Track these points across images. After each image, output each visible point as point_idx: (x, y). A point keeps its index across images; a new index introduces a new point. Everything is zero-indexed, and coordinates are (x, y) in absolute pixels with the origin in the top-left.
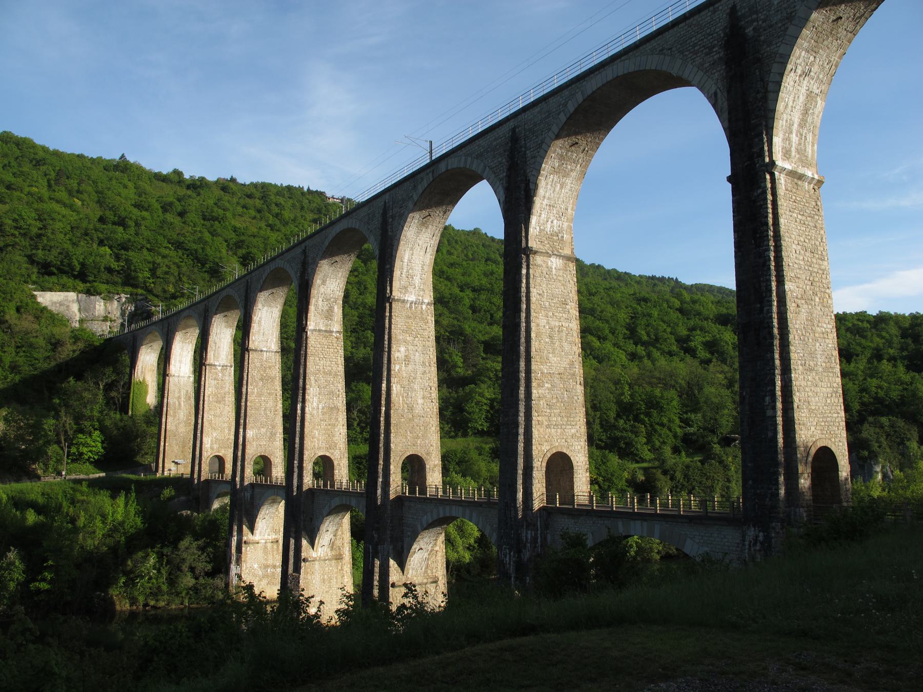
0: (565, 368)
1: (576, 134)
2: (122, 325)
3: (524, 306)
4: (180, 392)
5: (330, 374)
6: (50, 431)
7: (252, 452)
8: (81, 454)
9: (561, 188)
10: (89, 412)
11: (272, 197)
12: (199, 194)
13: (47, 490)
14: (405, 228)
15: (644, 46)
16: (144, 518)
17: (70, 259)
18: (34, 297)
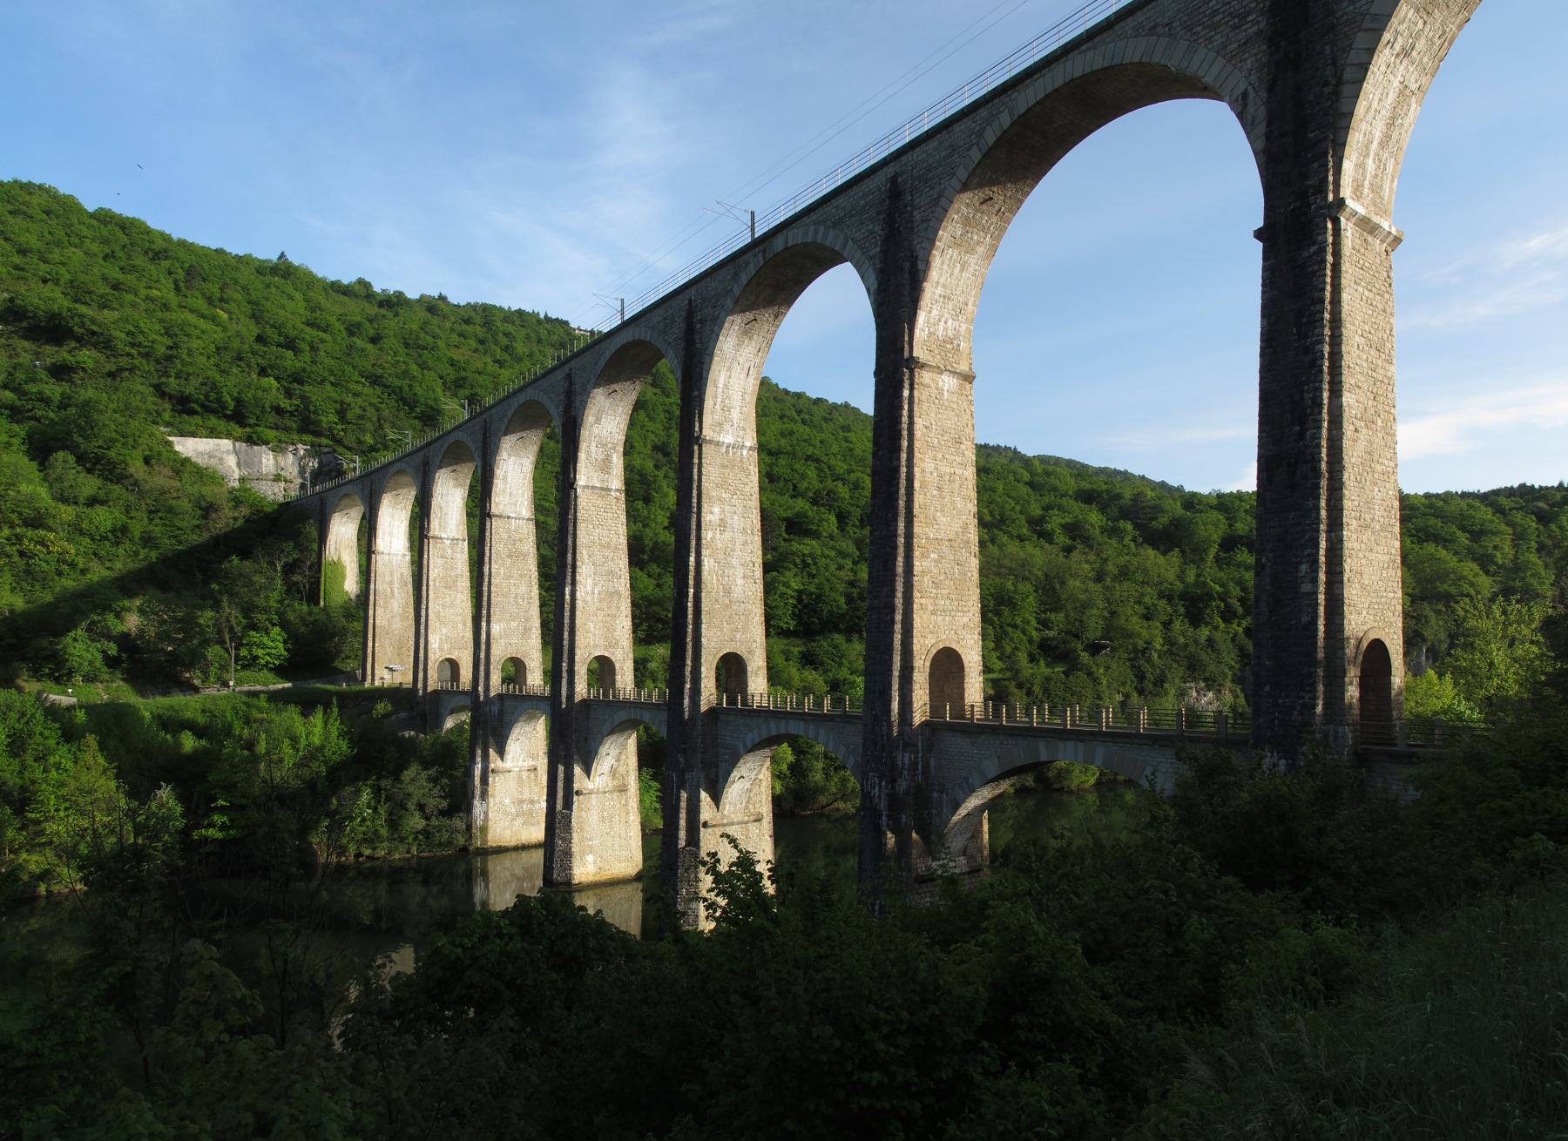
0: (957, 533)
1: (992, 183)
2: (303, 486)
3: (905, 444)
4: (392, 575)
5: (609, 548)
6: (208, 626)
7: (499, 652)
8: (256, 658)
9: (962, 270)
10: (262, 601)
11: (499, 324)
12: (397, 315)
13: (209, 705)
14: (721, 338)
15: (1123, 24)
16: (351, 740)
17: (219, 393)
18: (170, 444)
